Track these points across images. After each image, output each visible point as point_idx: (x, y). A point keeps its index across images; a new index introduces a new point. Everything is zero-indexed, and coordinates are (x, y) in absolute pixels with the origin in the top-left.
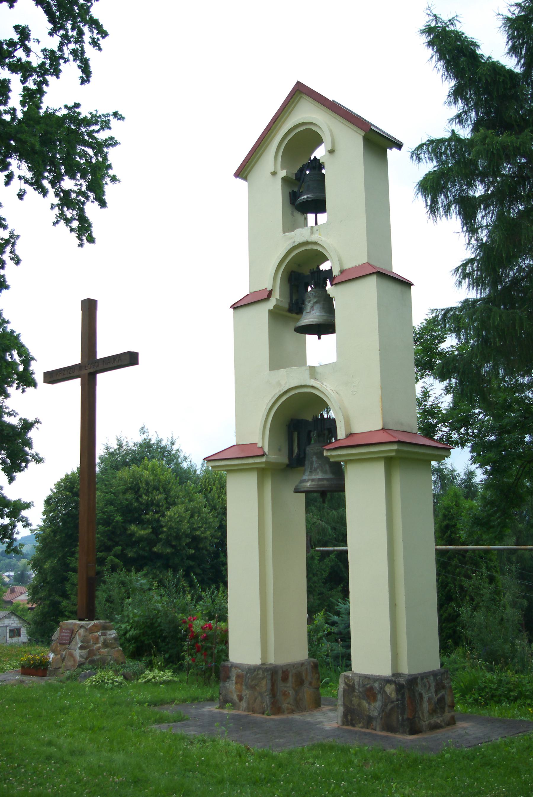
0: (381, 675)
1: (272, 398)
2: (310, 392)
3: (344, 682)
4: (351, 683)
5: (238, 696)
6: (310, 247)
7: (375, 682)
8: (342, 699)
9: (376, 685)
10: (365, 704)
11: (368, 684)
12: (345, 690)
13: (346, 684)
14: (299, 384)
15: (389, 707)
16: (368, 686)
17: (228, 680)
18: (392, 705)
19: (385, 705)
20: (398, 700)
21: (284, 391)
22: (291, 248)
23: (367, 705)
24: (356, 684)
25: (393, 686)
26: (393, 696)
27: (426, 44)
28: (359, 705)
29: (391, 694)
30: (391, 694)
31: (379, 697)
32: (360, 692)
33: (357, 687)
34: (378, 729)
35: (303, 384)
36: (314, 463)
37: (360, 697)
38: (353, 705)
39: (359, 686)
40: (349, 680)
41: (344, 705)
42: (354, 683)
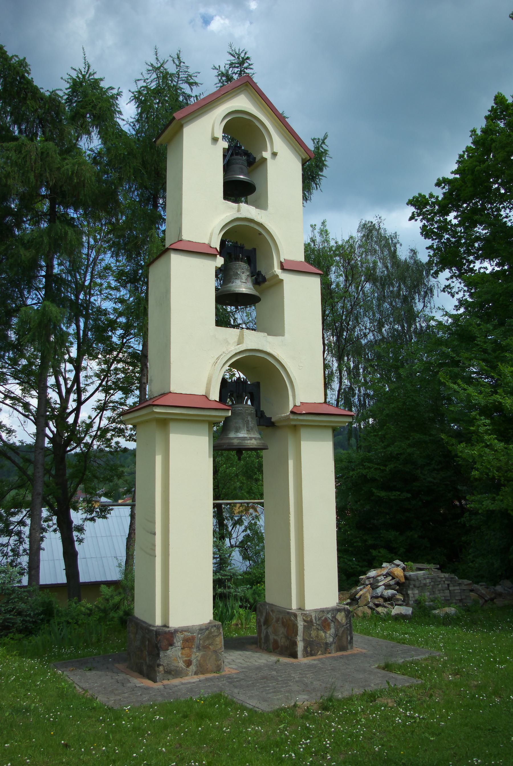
0: (328, 607)
1: (236, 354)
2: (263, 358)
3: (302, 620)
4: (309, 619)
5: (185, 662)
6: (252, 225)
7: (328, 613)
8: (302, 635)
9: (329, 616)
10: (322, 634)
11: (322, 617)
12: (305, 626)
13: (305, 621)
14: (257, 348)
15: (341, 630)
16: (323, 618)
17: (170, 648)
18: (343, 629)
19: (337, 630)
20: (347, 624)
21: (240, 350)
22: (237, 218)
23: (323, 634)
24: (313, 618)
25: (343, 613)
26: (344, 621)
27: (81, 66)
28: (317, 636)
29: (342, 620)
30: (342, 620)
31: (332, 625)
32: (318, 625)
33: (314, 621)
34: (333, 652)
35: (261, 349)
36: (250, 423)
37: (318, 629)
38: (312, 638)
39: (316, 620)
40: (307, 617)
41: (304, 640)
42: (311, 619)
